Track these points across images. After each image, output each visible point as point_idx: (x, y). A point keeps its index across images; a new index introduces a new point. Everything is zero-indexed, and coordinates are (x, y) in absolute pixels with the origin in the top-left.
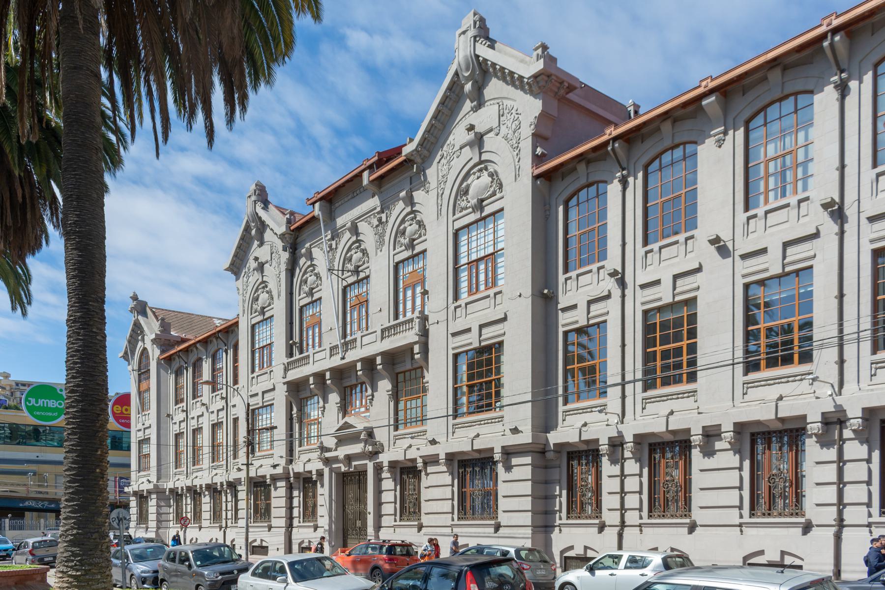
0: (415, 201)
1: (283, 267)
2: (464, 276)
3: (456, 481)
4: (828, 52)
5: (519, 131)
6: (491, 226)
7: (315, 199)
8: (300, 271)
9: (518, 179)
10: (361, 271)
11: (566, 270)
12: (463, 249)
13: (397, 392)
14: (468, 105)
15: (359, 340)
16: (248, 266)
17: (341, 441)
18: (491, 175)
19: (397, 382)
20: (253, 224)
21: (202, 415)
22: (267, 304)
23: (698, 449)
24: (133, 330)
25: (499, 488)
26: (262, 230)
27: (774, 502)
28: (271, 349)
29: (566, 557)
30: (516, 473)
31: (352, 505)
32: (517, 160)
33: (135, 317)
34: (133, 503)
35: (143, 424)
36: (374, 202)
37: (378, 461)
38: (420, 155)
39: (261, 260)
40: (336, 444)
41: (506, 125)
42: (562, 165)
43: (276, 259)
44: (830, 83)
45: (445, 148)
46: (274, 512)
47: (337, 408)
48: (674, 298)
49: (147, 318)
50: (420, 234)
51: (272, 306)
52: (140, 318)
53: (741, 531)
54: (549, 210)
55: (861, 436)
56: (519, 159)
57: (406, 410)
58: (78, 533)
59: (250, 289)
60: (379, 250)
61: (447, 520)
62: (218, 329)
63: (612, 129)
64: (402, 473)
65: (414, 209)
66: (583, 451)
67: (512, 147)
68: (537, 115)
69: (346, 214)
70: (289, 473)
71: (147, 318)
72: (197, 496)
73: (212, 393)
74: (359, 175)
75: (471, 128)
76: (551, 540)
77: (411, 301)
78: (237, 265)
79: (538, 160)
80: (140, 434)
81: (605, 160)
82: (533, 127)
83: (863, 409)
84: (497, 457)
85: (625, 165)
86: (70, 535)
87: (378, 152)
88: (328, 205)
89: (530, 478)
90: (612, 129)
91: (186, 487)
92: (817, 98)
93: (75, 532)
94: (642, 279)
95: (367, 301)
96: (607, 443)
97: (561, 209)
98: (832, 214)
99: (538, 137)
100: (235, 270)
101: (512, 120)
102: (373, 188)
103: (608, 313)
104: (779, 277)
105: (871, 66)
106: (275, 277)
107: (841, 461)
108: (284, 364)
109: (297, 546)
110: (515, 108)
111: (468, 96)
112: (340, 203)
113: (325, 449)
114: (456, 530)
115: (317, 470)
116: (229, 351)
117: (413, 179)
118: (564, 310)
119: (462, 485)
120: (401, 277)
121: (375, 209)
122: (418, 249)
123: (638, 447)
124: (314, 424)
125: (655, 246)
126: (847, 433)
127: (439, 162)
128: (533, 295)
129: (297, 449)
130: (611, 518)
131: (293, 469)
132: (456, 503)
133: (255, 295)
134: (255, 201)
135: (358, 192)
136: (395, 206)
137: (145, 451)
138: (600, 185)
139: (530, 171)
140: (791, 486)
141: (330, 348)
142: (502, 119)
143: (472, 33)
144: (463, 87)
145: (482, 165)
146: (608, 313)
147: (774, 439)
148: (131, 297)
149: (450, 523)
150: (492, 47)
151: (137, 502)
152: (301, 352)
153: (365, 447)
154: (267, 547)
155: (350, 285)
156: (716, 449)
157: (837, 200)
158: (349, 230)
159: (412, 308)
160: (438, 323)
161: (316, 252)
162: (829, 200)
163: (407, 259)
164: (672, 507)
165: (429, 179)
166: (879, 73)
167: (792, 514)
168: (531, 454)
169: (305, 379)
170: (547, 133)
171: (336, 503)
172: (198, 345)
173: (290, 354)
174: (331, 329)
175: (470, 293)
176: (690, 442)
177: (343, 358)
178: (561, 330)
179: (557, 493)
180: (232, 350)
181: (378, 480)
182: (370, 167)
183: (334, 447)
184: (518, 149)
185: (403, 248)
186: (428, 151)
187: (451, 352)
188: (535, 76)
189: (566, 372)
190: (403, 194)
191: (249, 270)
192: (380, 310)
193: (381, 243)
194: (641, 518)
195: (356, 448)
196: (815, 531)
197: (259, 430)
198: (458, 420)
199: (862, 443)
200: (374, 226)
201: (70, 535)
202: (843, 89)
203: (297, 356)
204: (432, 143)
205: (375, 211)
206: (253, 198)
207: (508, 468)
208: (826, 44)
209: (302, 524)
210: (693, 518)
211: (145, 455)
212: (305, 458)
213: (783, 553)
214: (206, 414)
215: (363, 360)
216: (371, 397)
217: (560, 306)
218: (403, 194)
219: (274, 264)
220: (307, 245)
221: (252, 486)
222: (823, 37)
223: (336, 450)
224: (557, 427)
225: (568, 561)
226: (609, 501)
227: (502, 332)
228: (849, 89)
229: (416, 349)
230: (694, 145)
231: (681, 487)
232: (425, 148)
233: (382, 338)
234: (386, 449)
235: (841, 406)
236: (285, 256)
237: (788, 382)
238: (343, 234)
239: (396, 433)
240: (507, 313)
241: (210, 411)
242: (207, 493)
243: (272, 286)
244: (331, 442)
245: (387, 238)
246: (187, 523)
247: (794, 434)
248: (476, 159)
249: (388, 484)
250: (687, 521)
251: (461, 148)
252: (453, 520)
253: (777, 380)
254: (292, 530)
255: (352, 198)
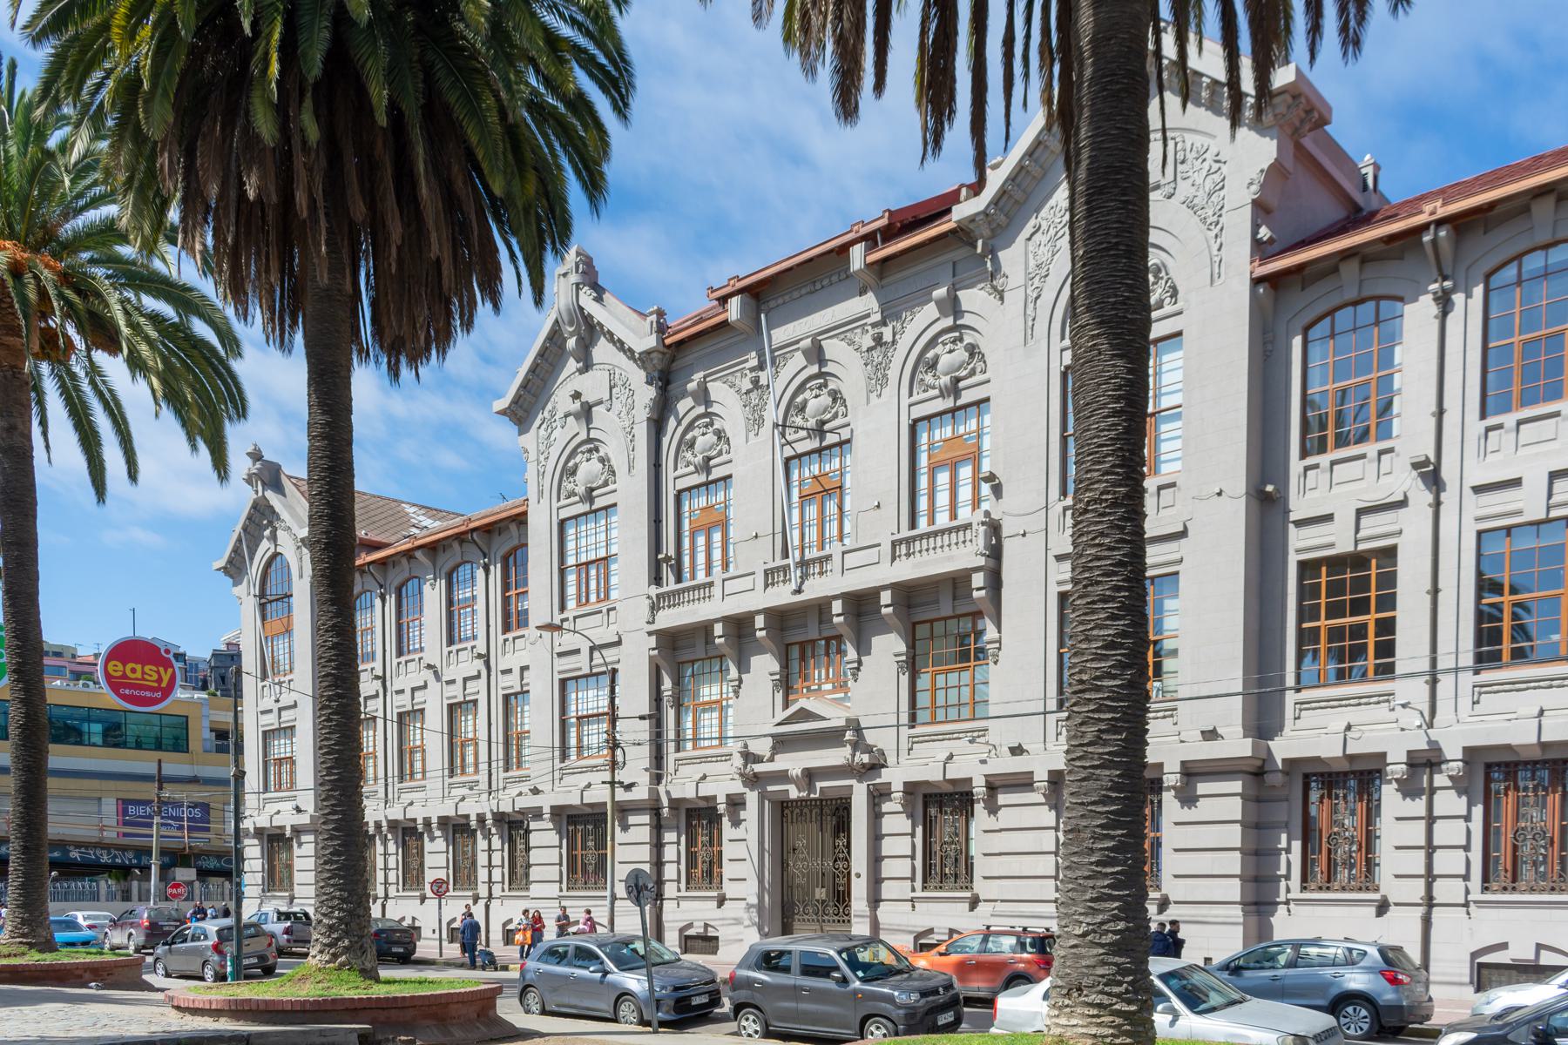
0: (964, 308)
1: (642, 414)
2: (571, 578)
3: (565, 841)
4: (1429, 250)
5: (1222, 193)
6: (603, 522)
7: (728, 290)
8: (679, 423)
9: (1217, 282)
10: (831, 431)
11: (1304, 454)
12: (571, 546)
13: (914, 658)
14: (572, 365)
15: (837, 559)
16: (549, 407)
17: (782, 743)
18: (602, 460)
19: (914, 640)
20: (571, 329)
21: (425, 687)
22: (601, 482)
23: (1173, 792)
24: (249, 518)
25: (724, 849)
26: (587, 342)
27: (1335, 873)
28: (607, 568)
29: (1480, 965)
30: (1204, 809)
31: (804, 859)
32: (1216, 246)
33: (257, 492)
34: (253, 852)
35: (277, 701)
36: (867, 303)
37: (878, 781)
38: (989, 223)
39: (588, 397)
40: (773, 748)
41: (1190, 181)
42: (1492, 205)
43: (623, 398)
44: (1427, 292)
45: (1044, 213)
46: (298, 877)
47: (771, 684)
48: (1356, 545)
49: (284, 495)
50: (721, 450)
51: (611, 487)
52: (270, 494)
53: (913, 907)
54: (1272, 342)
55: (1460, 785)
56: (1221, 245)
57: (934, 690)
58: (1127, 929)
59: (554, 452)
60: (752, 434)
61: (553, 889)
62: (472, 525)
63: (1439, 203)
64: (404, 835)
65: (958, 322)
66: (1338, 774)
67: (1205, 223)
68: (1265, 166)
69: (796, 323)
70: (658, 800)
71: (284, 495)
72: (412, 843)
73: (504, 632)
74: (844, 250)
75: (577, 395)
76: (1271, 927)
77: (719, 550)
78: (525, 406)
79: (1261, 250)
80: (270, 721)
81: (1402, 258)
82: (1255, 188)
83: (1464, 748)
84: (722, 808)
85: (1448, 271)
86: (1112, 932)
87: (889, 210)
88: (753, 302)
89: (1239, 818)
90: (1439, 203)
91: (389, 822)
92: (1408, 309)
93: (1121, 925)
94: (1480, 474)
95: (840, 487)
96: (1460, 757)
97: (1297, 342)
98: (1423, 476)
99: (1261, 209)
100: (520, 413)
101: (1204, 173)
102: (869, 278)
103: (1400, 532)
104: (1538, 523)
105: (1481, 278)
106: (621, 434)
107: (1431, 819)
108: (649, 597)
109: (676, 934)
110: (1213, 150)
111: (572, 354)
112: (780, 301)
113: (752, 758)
114: (564, 903)
115: (478, 815)
116: (492, 568)
117: (959, 267)
118: (1300, 523)
119: (571, 847)
120: (687, 514)
121: (868, 316)
122: (717, 473)
123: (909, 797)
124: (712, 710)
125: (1324, 460)
126: (1440, 780)
127: (1029, 239)
128: (1247, 493)
129: (671, 756)
130: (483, 890)
131: (668, 793)
132: (564, 869)
133: (571, 464)
134: (577, 285)
135: (825, 282)
136: (913, 314)
137: (280, 748)
138: (1383, 303)
139: (1248, 268)
140: (1360, 849)
141: (765, 571)
142: (1180, 168)
143: (574, 278)
144: (565, 340)
145: (591, 445)
146: (1400, 532)
147: (1313, 784)
148: (248, 454)
149: (556, 893)
150: (599, 299)
151: (262, 848)
152: (679, 580)
153: (853, 756)
154: (716, 938)
155: (799, 456)
156: (1199, 793)
157: (1432, 459)
158: (806, 353)
159: (929, 510)
160: (1024, 535)
161: (717, 390)
162: (1423, 458)
163: (698, 486)
164: (1343, 875)
165: (1005, 268)
166: (1310, 339)
167: (1360, 889)
168: (1240, 775)
169: (705, 628)
170: (1273, 202)
171: (772, 855)
172: (418, 554)
173: (657, 579)
174: (756, 537)
175: (579, 604)
176: (972, 795)
177: (799, 591)
178: (1293, 560)
179: (1283, 844)
180: (499, 566)
181: (875, 816)
182: (870, 239)
183: (768, 755)
184: (1219, 227)
185: (692, 468)
186: (1006, 215)
187: (557, 677)
188: (648, 353)
189: (1301, 633)
190: (940, 292)
191: (552, 416)
192: (878, 506)
193: (878, 378)
194: (913, 890)
195: (836, 756)
196: (982, 907)
197: (578, 718)
198: (919, 730)
199: (1460, 794)
200: (864, 349)
201: (1112, 932)
202: (1445, 303)
203: (670, 585)
204: (1016, 202)
205: (869, 321)
206: (574, 278)
207: (993, 809)
208: (1427, 238)
209: (401, 894)
210: (975, 891)
211: (280, 759)
212: (406, 798)
213: (1539, 947)
214: (434, 686)
215: (727, 620)
216: (855, 665)
217: (1293, 517)
218: (940, 292)
219: (617, 405)
220: (698, 376)
221: (565, 822)
222: (1425, 227)
223: (771, 760)
224: (1282, 730)
225: (1485, 972)
226: (482, 874)
227: (1177, 556)
228: (1453, 304)
229: (978, 580)
230: (1399, 304)
231: (1360, 845)
232: (1001, 210)
233: (893, 559)
234: (891, 760)
235: (1436, 742)
236: (650, 393)
237: (1359, 704)
238: (786, 359)
239: (451, 780)
240: (1188, 524)
241: (445, 678)
242: (438, 833)
243: (613, 448)
244: (762, 747)
245: (893, 373)
246: (442, 890)
247: (1365, 777)
248: (583, 436)
249: (896, 822)
250: (968, 894)
251: (566, 416)
252: (679, 890)
253: (1342, 701)
254: (662, 904)
255: (811, 293)
